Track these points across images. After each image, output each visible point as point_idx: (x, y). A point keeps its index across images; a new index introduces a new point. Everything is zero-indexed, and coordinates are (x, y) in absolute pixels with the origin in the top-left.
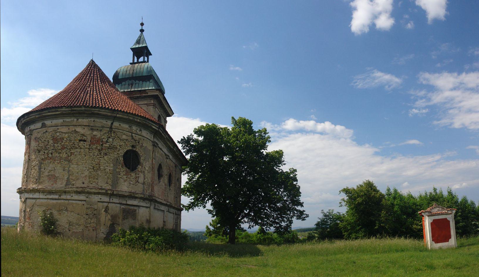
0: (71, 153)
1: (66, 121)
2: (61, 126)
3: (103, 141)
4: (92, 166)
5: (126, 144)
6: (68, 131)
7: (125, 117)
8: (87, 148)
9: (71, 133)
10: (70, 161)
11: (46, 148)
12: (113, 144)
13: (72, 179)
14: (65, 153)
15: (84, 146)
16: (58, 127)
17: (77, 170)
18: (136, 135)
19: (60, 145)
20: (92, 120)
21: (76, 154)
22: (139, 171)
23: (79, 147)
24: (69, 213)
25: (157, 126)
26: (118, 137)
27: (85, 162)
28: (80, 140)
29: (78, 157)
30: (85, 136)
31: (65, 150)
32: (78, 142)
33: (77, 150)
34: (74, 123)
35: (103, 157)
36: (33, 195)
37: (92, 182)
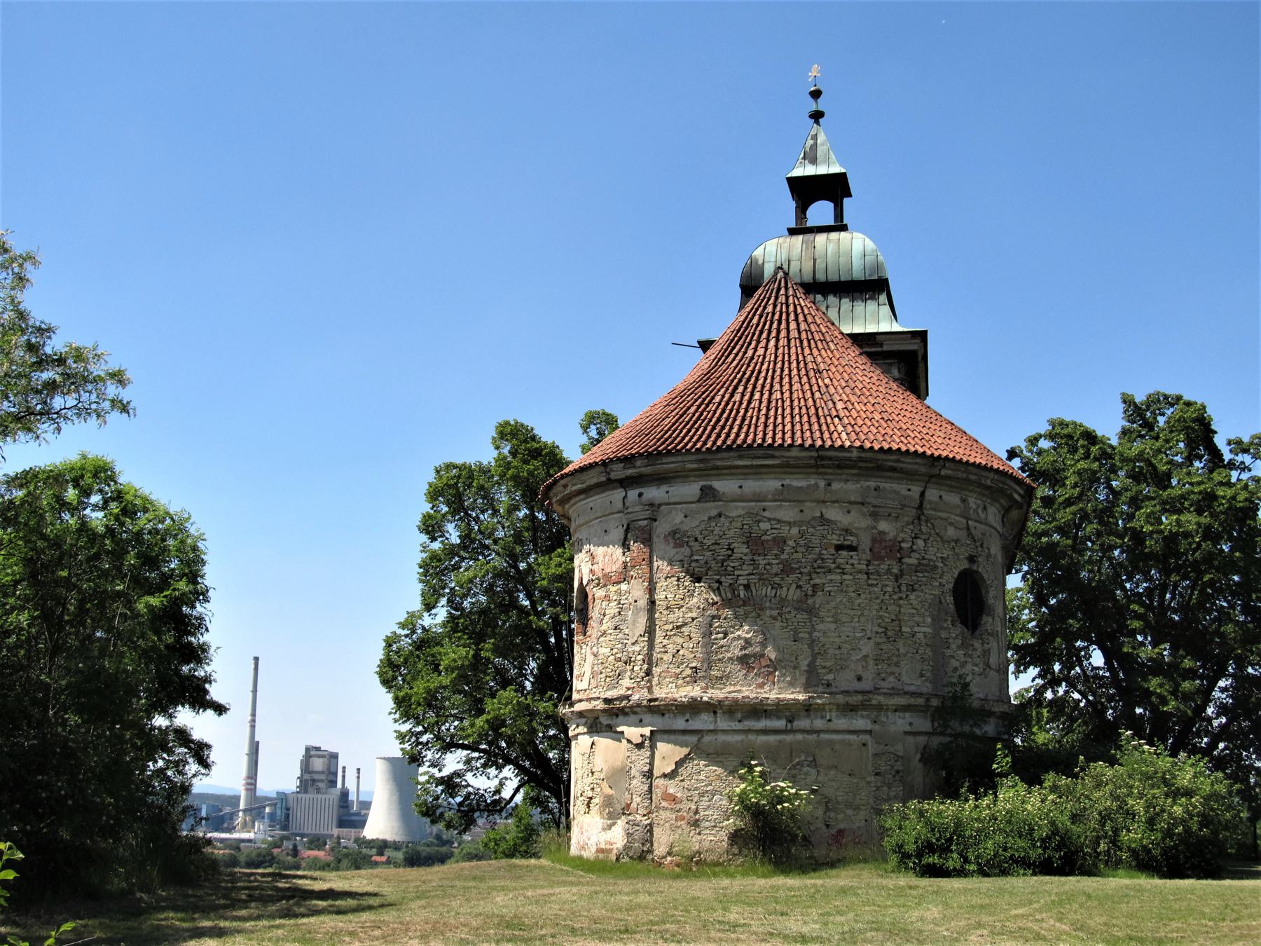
0: (814, 586)
1: (790, 487)
2: (775, 501)
3: (901, 548)
4: (882, 625)
5: (957, 554)
6: (799, 517)
7: (960, 475)
8: (860, 572)
9: (809, 523)
10: (811, 612)
11: (726, 570)
12: (926, 557)
13: (824, 667)
14: (794, 586)
15: (853, 565)
16: (764, 504)
17: (838, 640)
18: (977, 524)
19: (777, 561)
20: (872, 484)
21: (829, 589)
22: (989, 634)
23: (838, 567)
24: (822, 770)
25: (1022, 492)
26: (937, 534)
27: (860, 613)
28: (839, 548)
29: (838, 600)
30: (851, 534)
31: (793, 577)
32: (833, 551)
33: (833, 577)
34: (820, 495)
35: (907, 596)
36: (687, 721)
37: (883, 675)
